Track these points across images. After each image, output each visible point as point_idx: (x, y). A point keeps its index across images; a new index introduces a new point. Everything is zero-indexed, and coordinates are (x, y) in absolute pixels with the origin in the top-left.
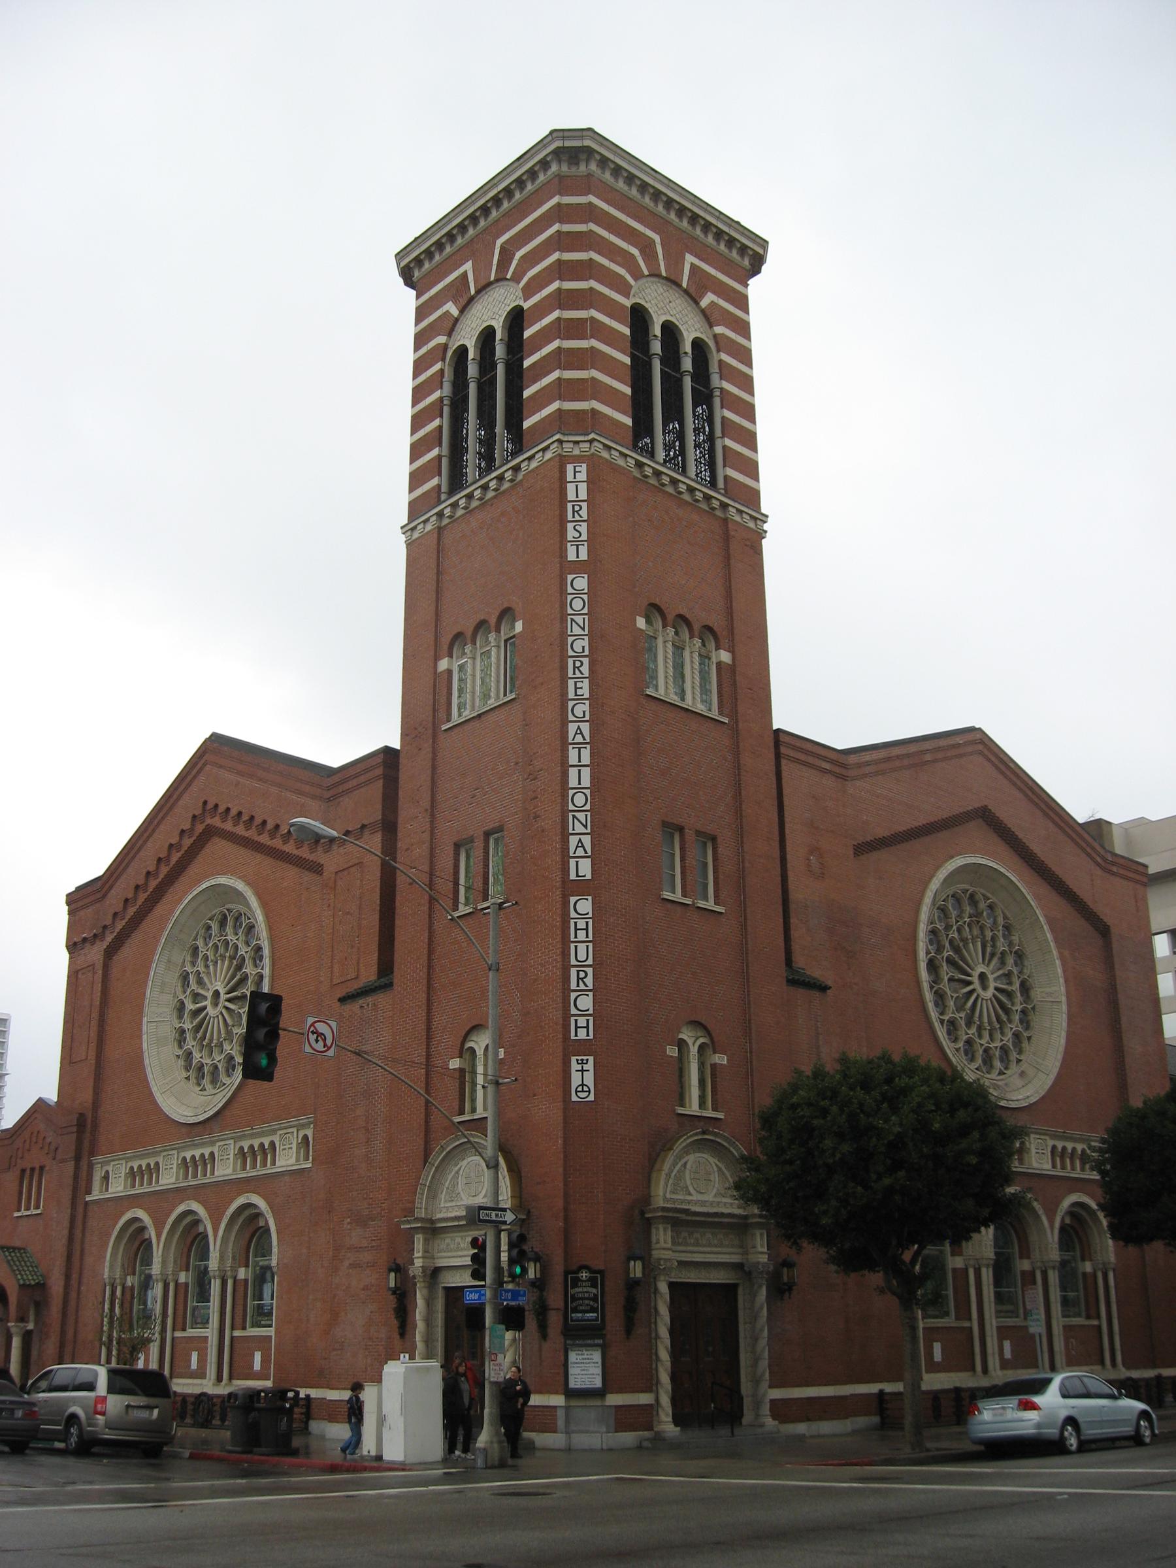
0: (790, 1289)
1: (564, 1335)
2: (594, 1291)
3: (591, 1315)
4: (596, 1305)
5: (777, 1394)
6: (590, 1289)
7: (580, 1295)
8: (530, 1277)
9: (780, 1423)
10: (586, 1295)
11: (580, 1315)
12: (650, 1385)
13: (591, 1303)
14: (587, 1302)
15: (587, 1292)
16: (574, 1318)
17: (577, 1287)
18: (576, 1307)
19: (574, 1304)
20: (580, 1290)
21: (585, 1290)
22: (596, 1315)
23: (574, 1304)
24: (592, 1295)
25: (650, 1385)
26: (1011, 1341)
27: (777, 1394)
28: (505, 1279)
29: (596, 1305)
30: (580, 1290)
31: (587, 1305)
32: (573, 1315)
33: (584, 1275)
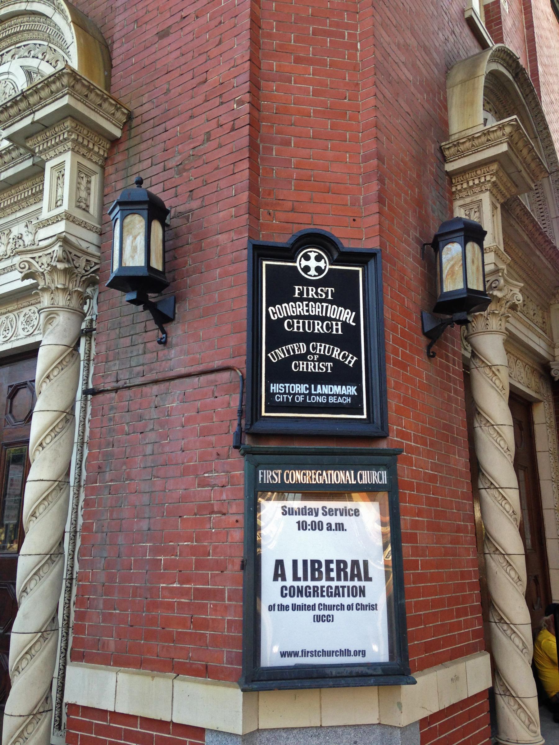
0: (452, 680)
1: (248, 452)
2: (347, 316)
3: (337, 389)
4: (351, 361)
5: (293, 82)
6: (334, 311)
7: (298, 326)
8: (129, 262)
9: (549, 362)
10: (319, 327)
11: (301, 388)
12: (421, 570)
13: (337, 353)
14: (322, 348)
15: (323, 319)
16: (279, 399)
17: (289, 298)
18: (287, 361)
19: (280, 354)
20: (300, 309)
21: (316, 309)
22: (352, 390)
23: (280, 354)
24: (336, 329)
25: (421, 570)
26: (380, 504)
27: (293, 82)
28: (284, 348)
29: (351, 361)
30: (300, 309)
31: (323, 358)
32: (275, 388)
33: (313, 264)
